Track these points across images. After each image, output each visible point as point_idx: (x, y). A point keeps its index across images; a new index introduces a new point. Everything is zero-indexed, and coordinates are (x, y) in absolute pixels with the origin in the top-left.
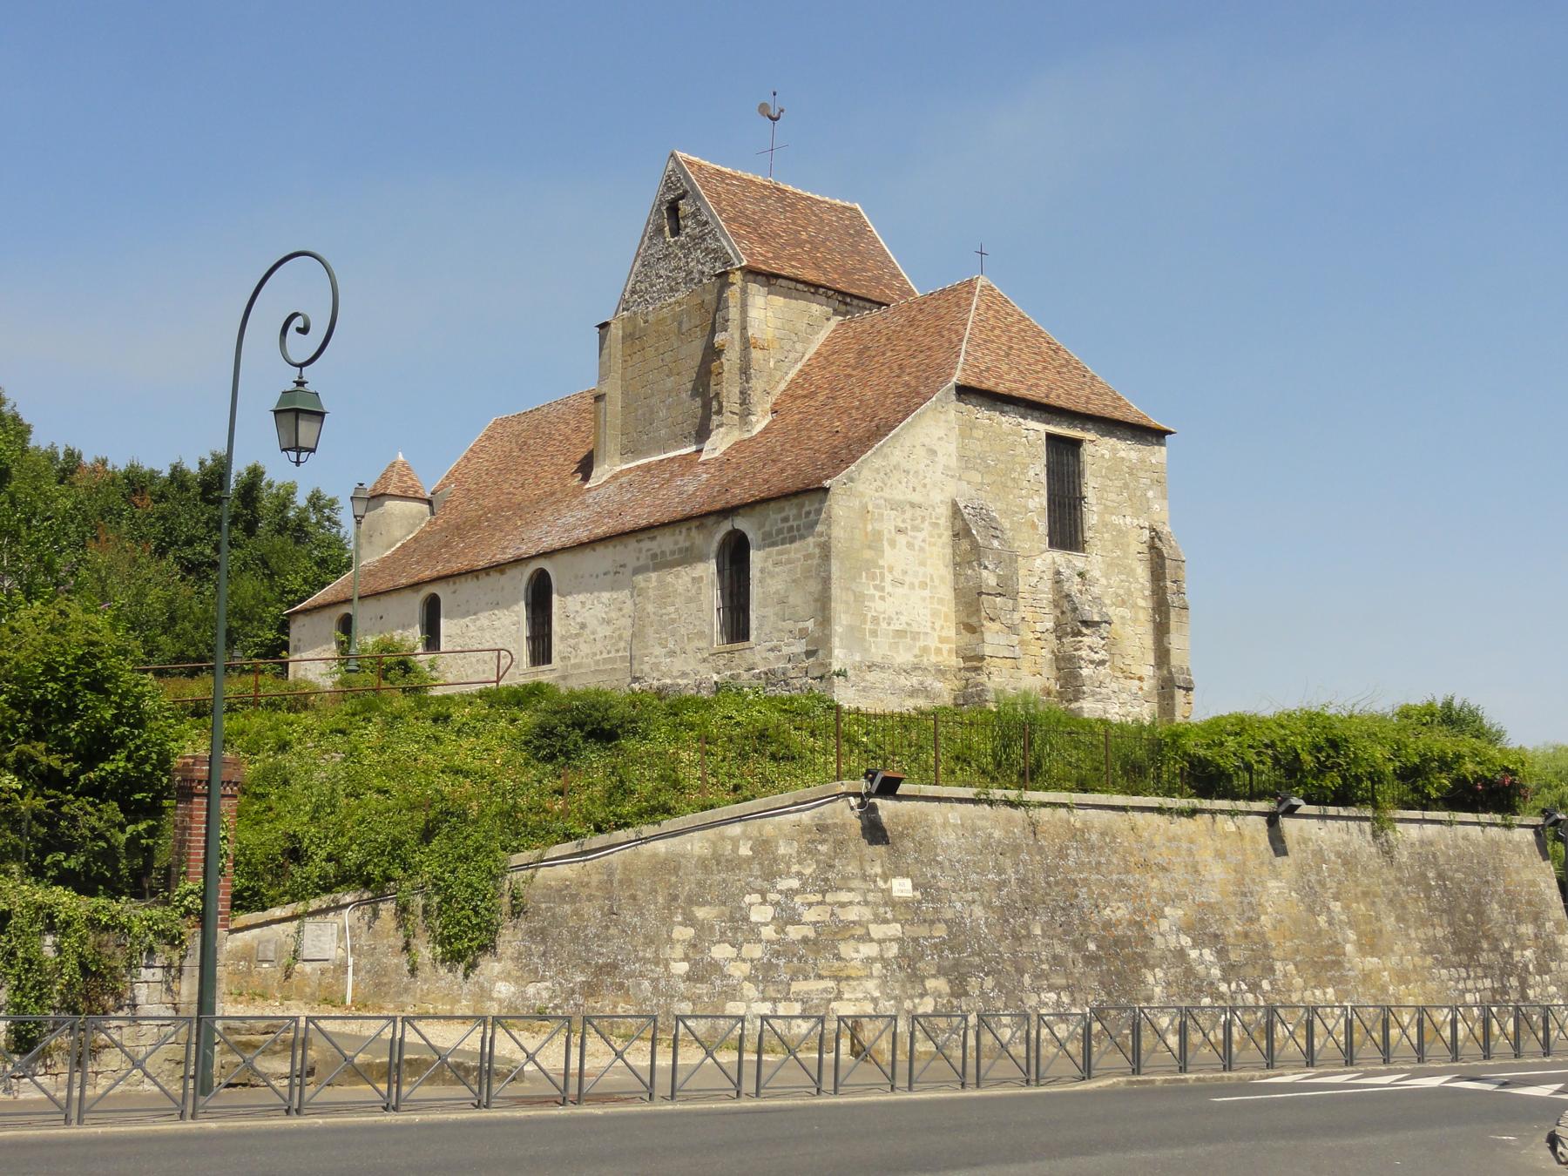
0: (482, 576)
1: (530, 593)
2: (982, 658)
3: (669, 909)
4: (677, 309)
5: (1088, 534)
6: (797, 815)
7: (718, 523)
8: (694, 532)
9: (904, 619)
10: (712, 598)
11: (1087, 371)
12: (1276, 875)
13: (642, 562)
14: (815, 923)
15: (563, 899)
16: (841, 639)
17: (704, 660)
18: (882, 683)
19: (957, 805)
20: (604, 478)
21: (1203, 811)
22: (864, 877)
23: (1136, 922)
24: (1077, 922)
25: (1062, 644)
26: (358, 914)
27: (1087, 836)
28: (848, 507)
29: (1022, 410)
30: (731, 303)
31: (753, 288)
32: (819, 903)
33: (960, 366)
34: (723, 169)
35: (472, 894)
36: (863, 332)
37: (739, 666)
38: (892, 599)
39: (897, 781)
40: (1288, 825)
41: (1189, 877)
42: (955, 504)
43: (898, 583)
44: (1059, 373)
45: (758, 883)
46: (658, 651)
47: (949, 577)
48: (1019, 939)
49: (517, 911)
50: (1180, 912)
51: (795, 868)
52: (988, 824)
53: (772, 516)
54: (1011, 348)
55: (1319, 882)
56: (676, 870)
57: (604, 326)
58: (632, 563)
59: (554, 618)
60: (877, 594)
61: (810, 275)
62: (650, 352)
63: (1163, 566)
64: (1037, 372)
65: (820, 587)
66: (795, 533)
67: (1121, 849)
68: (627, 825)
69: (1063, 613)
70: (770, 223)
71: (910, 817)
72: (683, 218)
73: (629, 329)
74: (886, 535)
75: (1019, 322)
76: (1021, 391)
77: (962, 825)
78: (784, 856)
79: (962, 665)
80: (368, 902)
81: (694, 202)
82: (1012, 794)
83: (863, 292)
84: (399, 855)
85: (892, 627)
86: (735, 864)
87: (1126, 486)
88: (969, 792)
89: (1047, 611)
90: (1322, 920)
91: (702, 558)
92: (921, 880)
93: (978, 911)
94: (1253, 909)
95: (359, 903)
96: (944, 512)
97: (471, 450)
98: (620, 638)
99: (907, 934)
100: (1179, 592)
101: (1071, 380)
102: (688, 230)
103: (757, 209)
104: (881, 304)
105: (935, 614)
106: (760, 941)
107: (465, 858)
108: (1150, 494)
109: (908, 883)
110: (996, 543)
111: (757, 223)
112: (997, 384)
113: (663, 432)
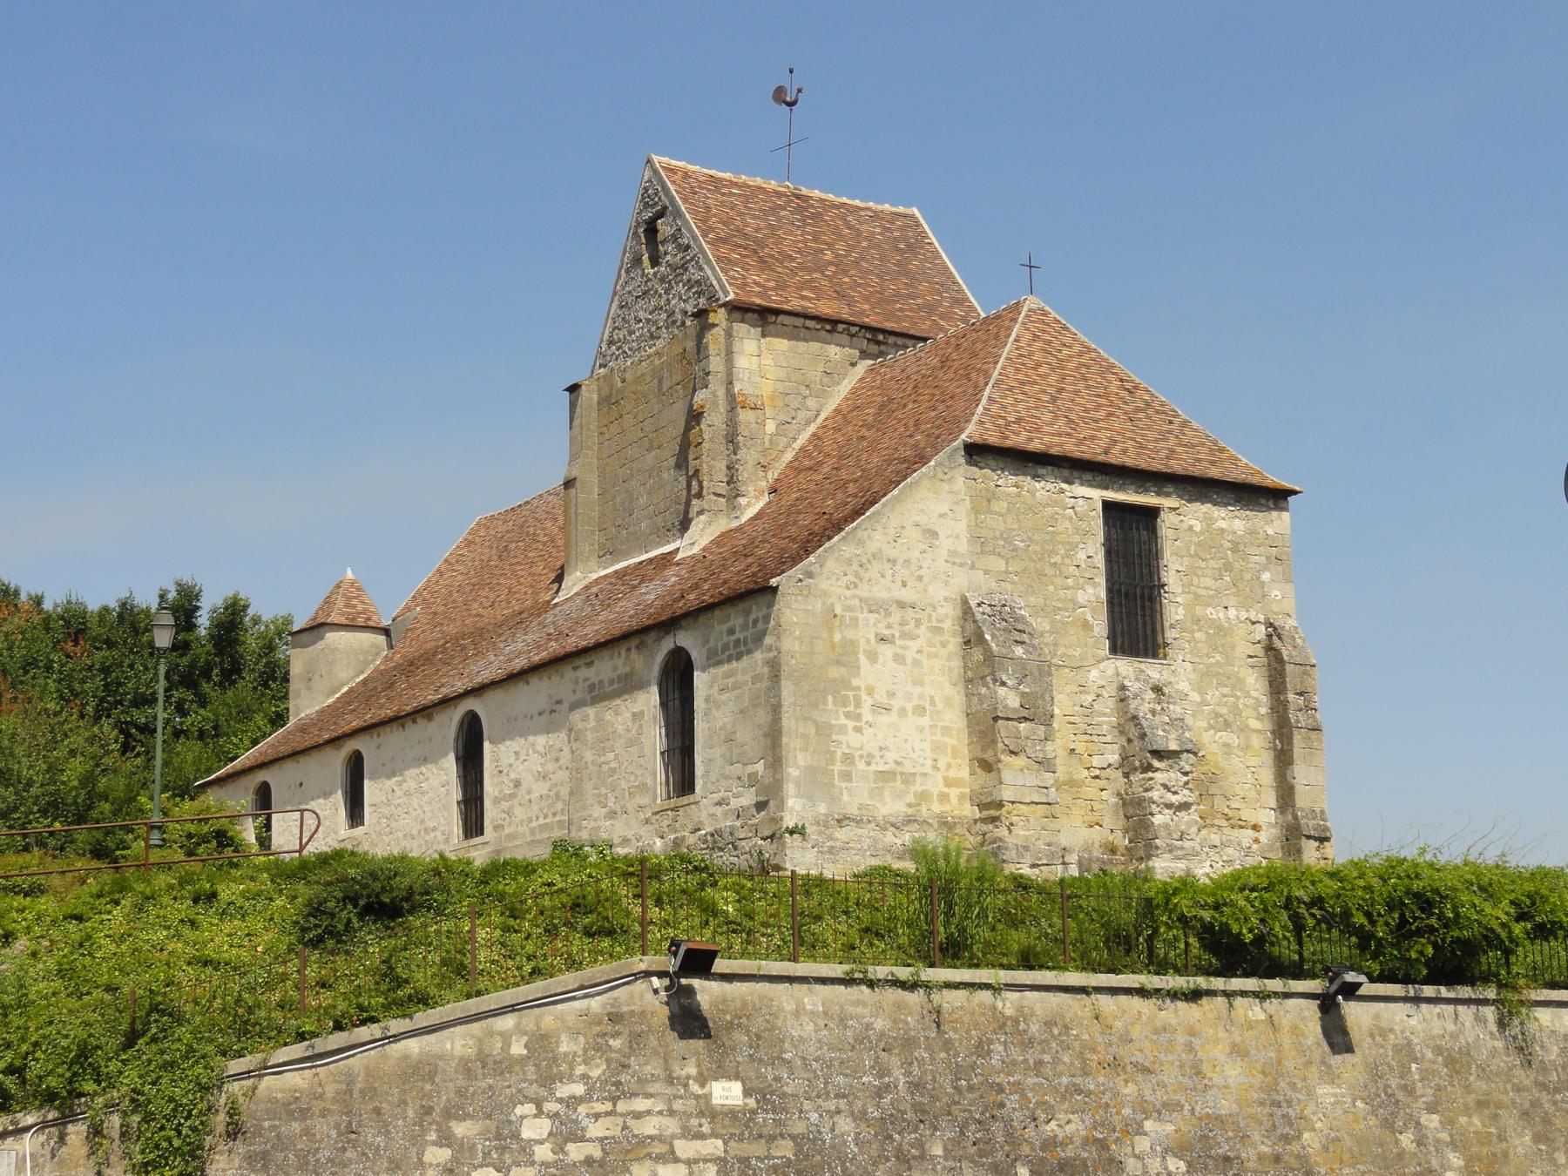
0: (409, 724)
1: (460, 743)
2: (1000, 805)
3: (421, 1126)
4: (657, 362)
5: (1170, 634)
6: (586, 1001)
7: (658, 640)
8: (634, 654)
9: (890, 756)
10: (655, 738)
12: (1332, 1077)
13: (579, 695)
14: (601, 1140)
15: (291, 1113)
16: (798, 785)
17: (647, 821)
18: (859, 841)
19: (818, 987)
20: (576, 590)
21: (1211, 993)
22: (670, 1080)
23: (1096, 1140)
24: (1000, 1139)
25: (1130, 783)
26: (42, 1138)
27: (1022, 1026)
28: (806, 611)
29: (1066, 473)
30: (712, 350)
31: (741, 328)
32: (608, 1114)
33: (975, 418)
35: (174, 1110)
36: (892, 378)
37: (684, 826)
38: (871, 730)
39: (710, 956)
40: (1354, 1012)
41: (1185, 1081)
42: (965, 601)
43: (879, 708)
45: (533, 1090)
46: (598, 812)
47: (958, 697)
48: (908, 1161)
49: (234, 1132)
50: (1170, 1128)
51: (580, 1070)
52: (866, 1012)
53: (718, 628)
55: (1405, 1088)
56: (431, 1076)
57: (574, 389)
58: (569, 698)
59: (486, 774)
60: (851, 724)
61: (826, 308)
62: (628, 420)
64: (1096, 421)
65: (770, 717)
66: (743, 648)
67: (1077, 1044)
68: (373, 1020)
69: (1129, 741)
70: (779, 241)
71: (744, 1003)
72: (663, 242)
73: (605, 393)
74: (863, 646)
75: (1081, 354)
77: (826, 1013)
78: (566, 1054)
79: (978, 815)
80: (54, 1123)
81: (674, 220)
82: (903, 973)
83: (904, 326)
84: (90, 1064)
85: (873, 767)
86: (505, 1066)
87: (1228, 567)
88: (838, 970)
89: (1109, 739)
90: (1407, 1140)
91: (642, 686)
92: (756, 1084)
93: (845, 1125)
94: (1291, 1125)
95: (43, 1125)
96: (948, 614)
97: (446, 561)
98: (557, 796)
99: (732, 1153)
100: (1308, 707)
101: (1149, 428)
102: (668, 257)
103: (762, 224)
104: (925, 339)
105: (938, 748)
106: (533, 1163)
107: (170, 1066)
108: (1266, 576)
109: (736, 1088)
111: (761, 244)
112: (1030, 439)
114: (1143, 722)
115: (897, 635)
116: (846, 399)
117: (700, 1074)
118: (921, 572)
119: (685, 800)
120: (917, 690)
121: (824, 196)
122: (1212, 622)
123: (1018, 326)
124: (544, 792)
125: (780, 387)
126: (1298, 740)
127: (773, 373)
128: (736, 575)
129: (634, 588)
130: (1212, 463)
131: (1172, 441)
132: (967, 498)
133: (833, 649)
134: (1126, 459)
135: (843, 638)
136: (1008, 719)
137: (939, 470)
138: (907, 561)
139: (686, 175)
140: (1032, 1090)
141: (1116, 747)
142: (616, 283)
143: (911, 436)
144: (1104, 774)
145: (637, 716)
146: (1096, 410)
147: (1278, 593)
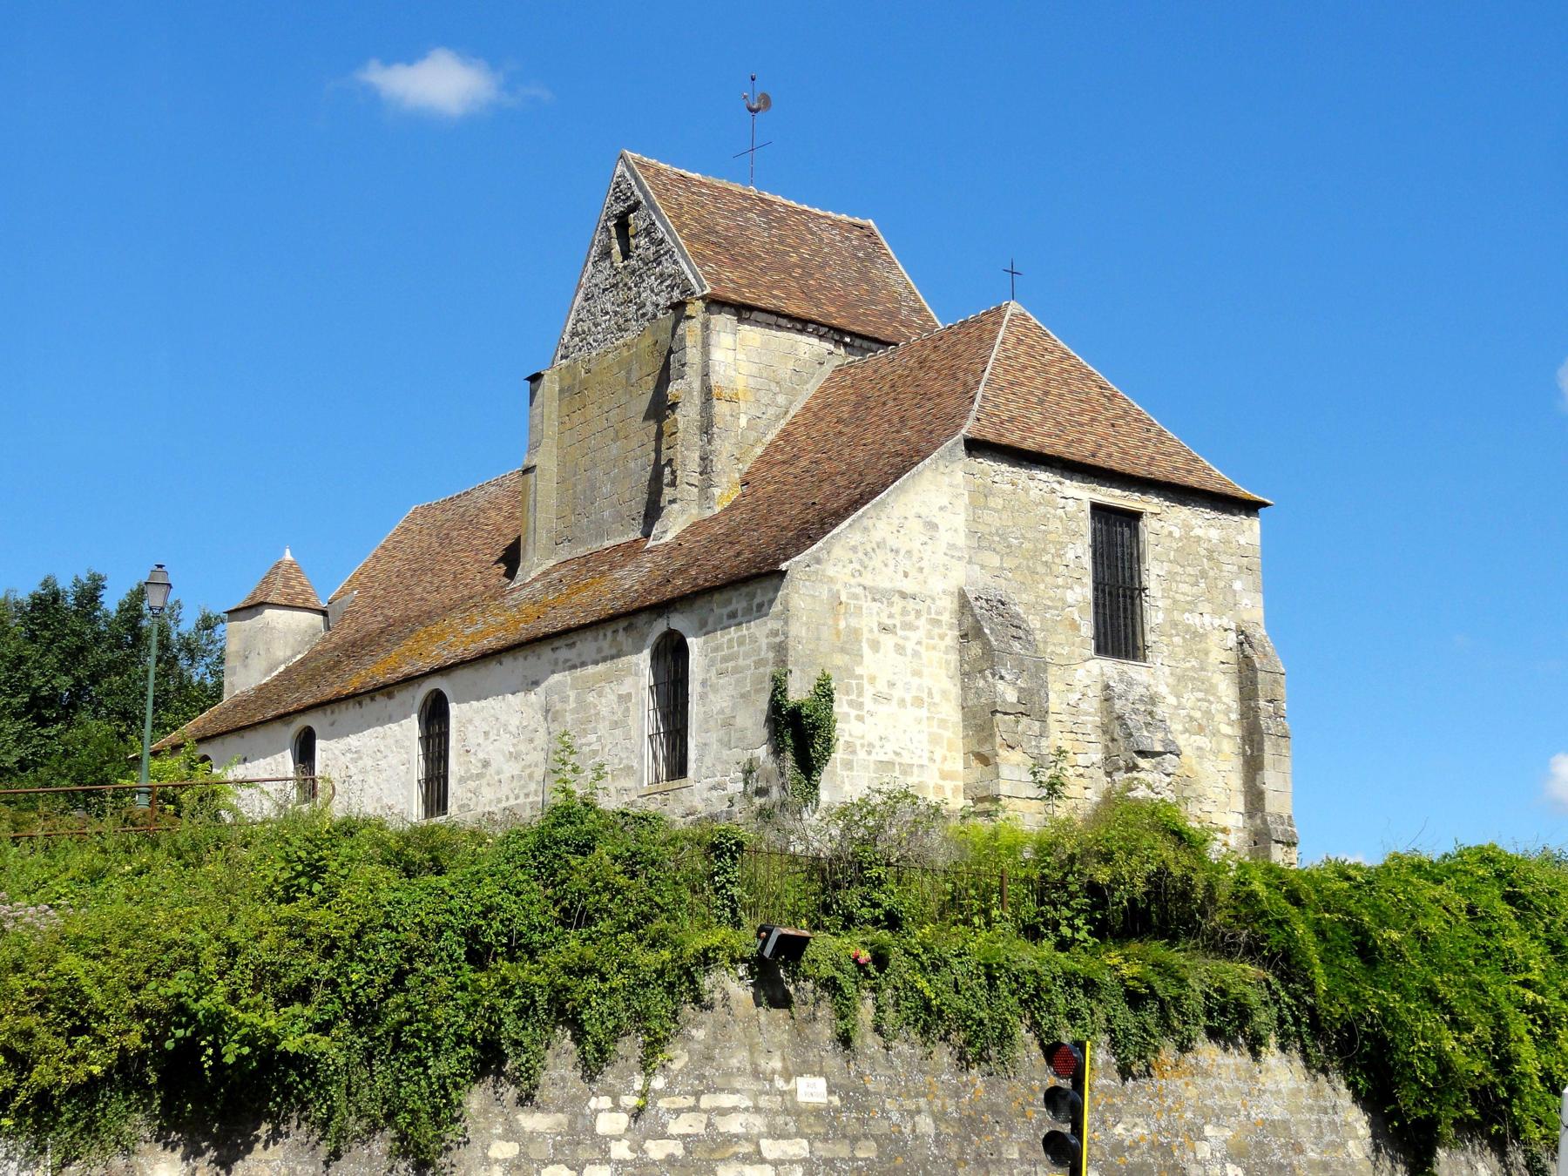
0: (366, 701)
2: (996, 799)
5: (1150, 638)
7: (650, 623)
8: (621, 636)
9: (890, 747)
10: (644, 717)
11: (1153, 425)
14: (684, 1137)
20: (533, 575)
22: (756, 1074)
30: (689, 342)
33: (973, 414)
34: (689, 174)
36: (864, 379)
42: (962, 595)
43: (878, 697)
44: (1113, 425)
47: (955, 690)
48: (985, 1165)
53: (717, 611)
54: (1046, 393)
60: (853, 713)
61: (793, 308)
62: (592, 410)
63: (1254, 682)
64: (1081, 425)
74: (866, 635)
75: (1061, 360)
76: (1058, 448)
83: (868, 330)
85: (874, 757)
89: (1092, 738)
96: (949, 605)
98: (531, 776)
100: (1277, 715)
104: (886, 344)
105: (935, 740)
106: (609, 1161)
109: (821, 1083)
110: (1016, 646)
112: (1024, 439)
113: (606, 514)
114: (1129, 722)
115: (898, 625)
116: (815, 397)
117: (785, 1068)
118: (922, 564)
119: (676, 784)
120: (915, 681)
121: (785, 202)
122: (1188, 629)
123: (1003, 329)
124: (516, 772)
125: (751, 382)
126: (1268, 746)
127: (745, 368)
128: (726, 561)
129: (603, 574)
130: (1189, 472)
131: (1151, 449)
132: (966, 493)
133: (839, 637)
134: (1112, 463)
135: (847, 626)
136: (1006, 714)
137: (941, 462)
138: (909, 552)
139: (658, 172)
140: (1102, 1091)
141: (1100, 746)
142: (582, 276)
143: (898, 432)
144: (1087, 772)
145: (624, 699)
146: (1080, 414)
147: (1248, 602)
